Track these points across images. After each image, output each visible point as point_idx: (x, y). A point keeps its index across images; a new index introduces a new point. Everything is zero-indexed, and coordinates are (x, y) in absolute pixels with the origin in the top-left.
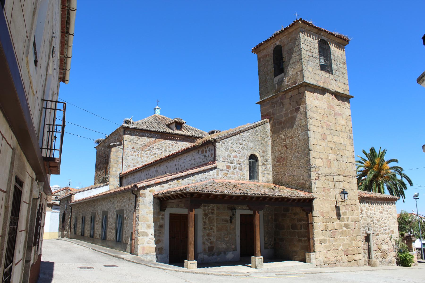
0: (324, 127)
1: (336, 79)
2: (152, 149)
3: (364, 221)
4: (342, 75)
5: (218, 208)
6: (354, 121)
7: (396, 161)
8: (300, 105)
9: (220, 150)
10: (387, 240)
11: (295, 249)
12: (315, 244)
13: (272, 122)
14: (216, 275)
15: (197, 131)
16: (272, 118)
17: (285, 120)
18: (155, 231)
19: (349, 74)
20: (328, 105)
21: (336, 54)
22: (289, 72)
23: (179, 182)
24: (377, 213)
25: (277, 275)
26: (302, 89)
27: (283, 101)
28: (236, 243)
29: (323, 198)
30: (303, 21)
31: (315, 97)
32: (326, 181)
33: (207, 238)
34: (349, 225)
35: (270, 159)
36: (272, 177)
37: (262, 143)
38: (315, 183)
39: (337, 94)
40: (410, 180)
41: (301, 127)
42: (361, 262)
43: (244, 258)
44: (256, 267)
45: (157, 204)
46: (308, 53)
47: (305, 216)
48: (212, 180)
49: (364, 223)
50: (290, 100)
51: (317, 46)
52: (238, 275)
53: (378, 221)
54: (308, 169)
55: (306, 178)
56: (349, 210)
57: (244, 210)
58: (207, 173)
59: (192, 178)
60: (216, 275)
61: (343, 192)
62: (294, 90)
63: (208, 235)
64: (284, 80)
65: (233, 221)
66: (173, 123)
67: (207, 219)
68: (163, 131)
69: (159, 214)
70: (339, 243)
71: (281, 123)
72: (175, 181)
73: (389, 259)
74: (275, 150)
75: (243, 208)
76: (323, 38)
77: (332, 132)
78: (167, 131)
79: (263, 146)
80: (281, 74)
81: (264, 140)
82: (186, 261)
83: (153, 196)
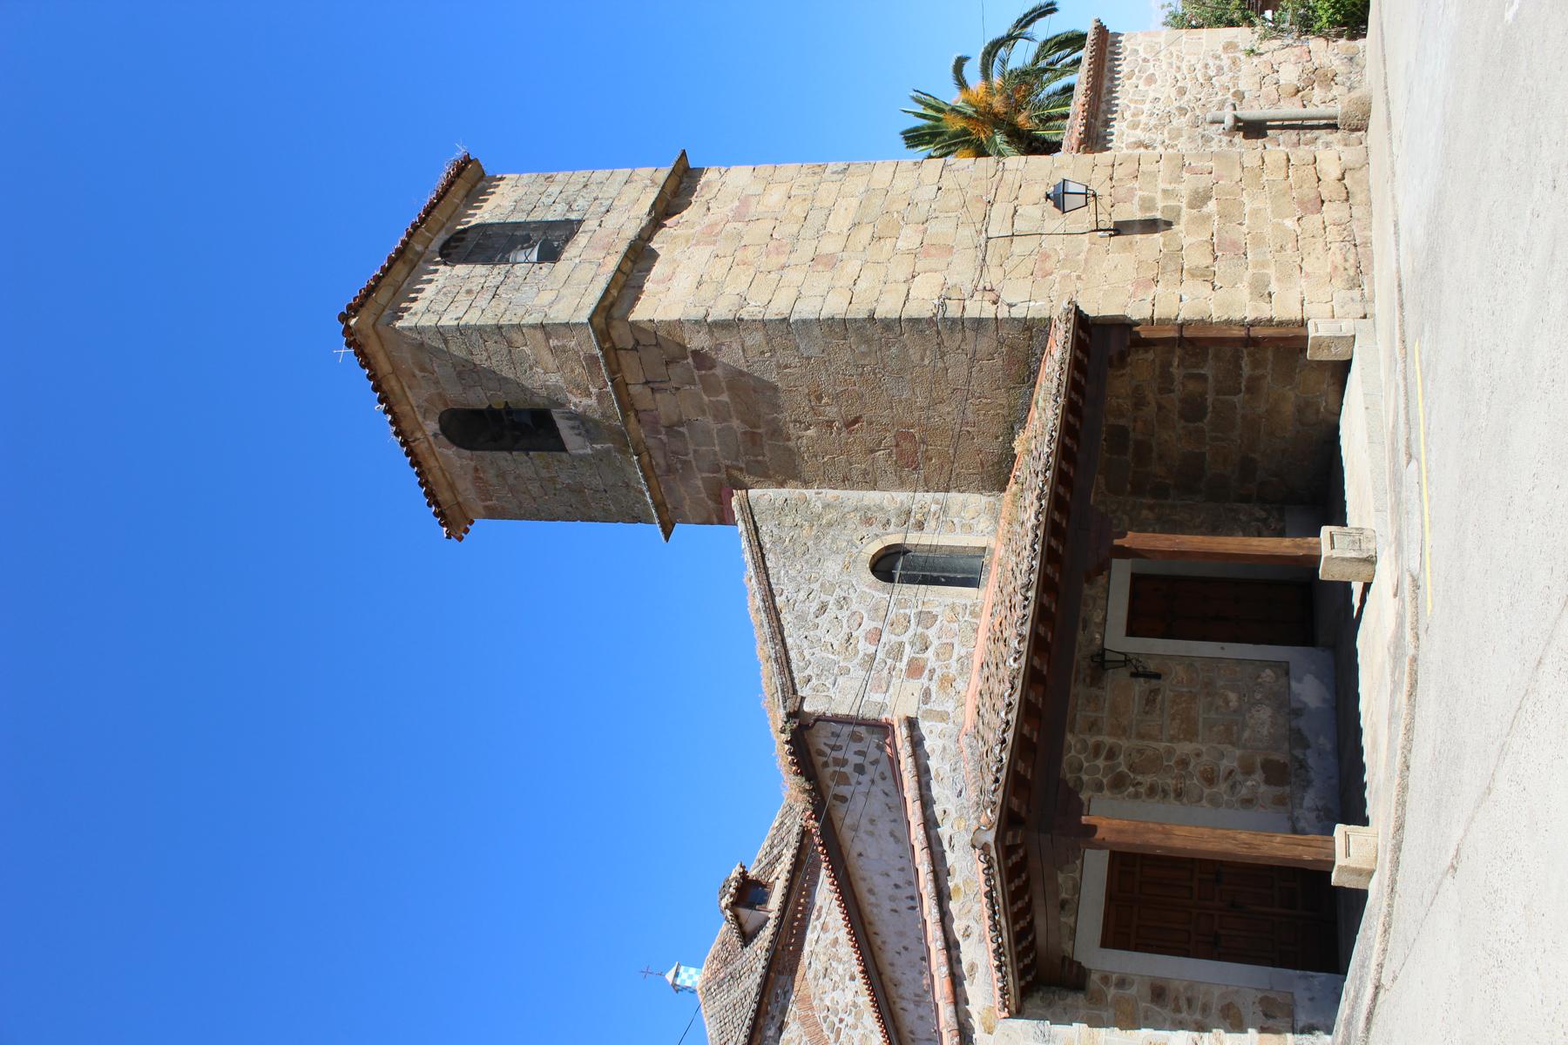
0: (783, 259)
1: (604, 209)
2: (832, 1017)
3: (1182, 139)
4: (594, 187)
5: (1093, 726)
6: (776, 156)
7: (960, 63)
8: (684, 347)
9: (838, 697)
10: (1261, 67)
11: (1288, 409)
12: (1271, 320)
13: (747, 479)
14: (1409, 729)
15: (782, 823)
16: (729, 476)
17: (743, 421)
18: (1179, 1025)
19: (594, 166)
20: (698, 243)
21: (508, 204)
22: (547, 388)
23: (957, 888)
24: (1152, 95)
25: (1410, 457)
26: (619, 333)
27: (663, 421)
28: (1252, 662)
29: (1079, 278)
30: (354, 309)
31: (661, 287)
32: (1008, 265)
33: (1223, 787)
34: (1197, 192)
35: (901, 497)
36: (977, 496)
37: (830, 525)
38: (1011, 306)
39: (661, 208)
40: (1034, 10)
41: (773, 351)
42: (1351, 155)
43: (1318, 618)
44: (1371, 561)
45: (1050, 1005)
46: (482, 302)
47: (1150, 355)
48: (964, 741)
49: (1191, 139)
50: (659, 390)
51: (461, 269)
52: (1413, 625)
53: (1182, 92)
54: (952, 330)
55: (985, 344)
56: (1132, 189)
57: (1110, 620)
58: (933, 764)
59: (944, 831)
60: (1409, 729)
61: (1058, 199)
62: (620, 370)
63: (1210, 779)
64: (580, 410)
65: (1152, 666)
66: (736, 917)
67: (1139, 778)
68: (763, 962)
69: (1097, 1000)
70: (1268, 230)
71: (753, 438)
72: (953, 906)
73: (1337, 62)
74: (865, 473)
75: (1098, 620)
76: (436, 244)
77: (808, 233)
78: (766, 944)
79: (842, 520)
80: (553, 422)
81: (819, 516)
82: (1335, 879)
83: (1011, 1016)
